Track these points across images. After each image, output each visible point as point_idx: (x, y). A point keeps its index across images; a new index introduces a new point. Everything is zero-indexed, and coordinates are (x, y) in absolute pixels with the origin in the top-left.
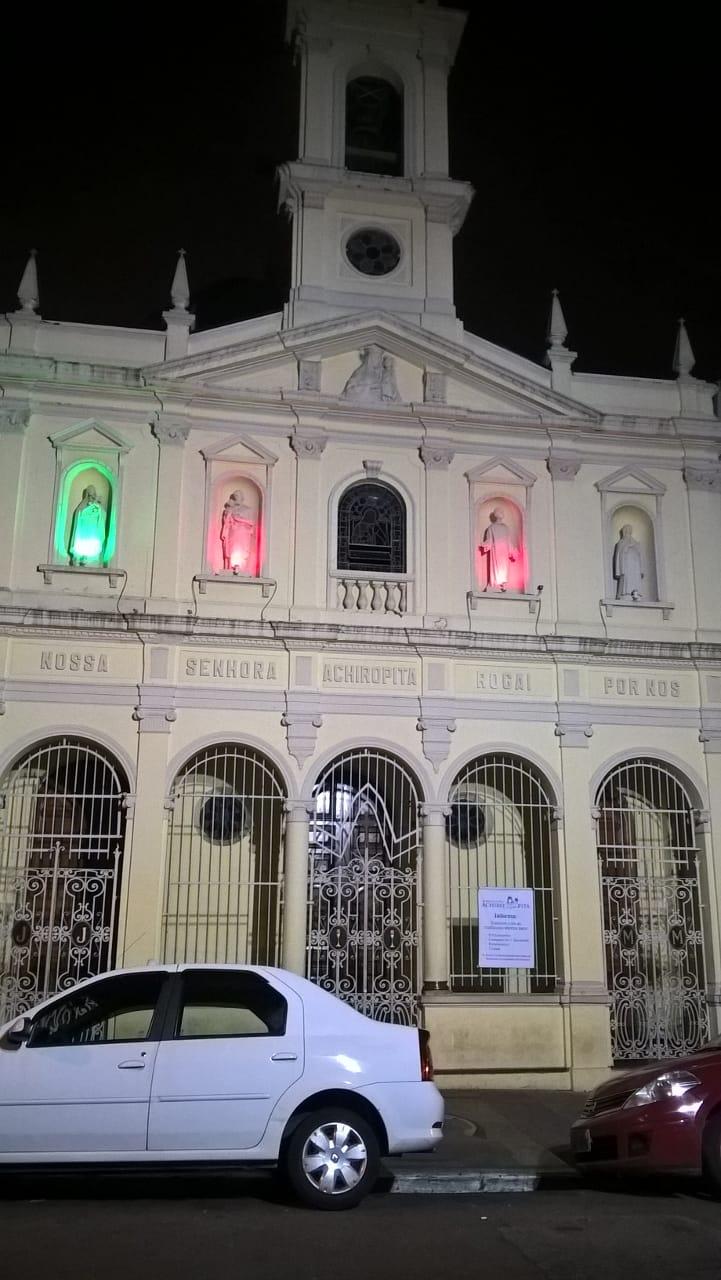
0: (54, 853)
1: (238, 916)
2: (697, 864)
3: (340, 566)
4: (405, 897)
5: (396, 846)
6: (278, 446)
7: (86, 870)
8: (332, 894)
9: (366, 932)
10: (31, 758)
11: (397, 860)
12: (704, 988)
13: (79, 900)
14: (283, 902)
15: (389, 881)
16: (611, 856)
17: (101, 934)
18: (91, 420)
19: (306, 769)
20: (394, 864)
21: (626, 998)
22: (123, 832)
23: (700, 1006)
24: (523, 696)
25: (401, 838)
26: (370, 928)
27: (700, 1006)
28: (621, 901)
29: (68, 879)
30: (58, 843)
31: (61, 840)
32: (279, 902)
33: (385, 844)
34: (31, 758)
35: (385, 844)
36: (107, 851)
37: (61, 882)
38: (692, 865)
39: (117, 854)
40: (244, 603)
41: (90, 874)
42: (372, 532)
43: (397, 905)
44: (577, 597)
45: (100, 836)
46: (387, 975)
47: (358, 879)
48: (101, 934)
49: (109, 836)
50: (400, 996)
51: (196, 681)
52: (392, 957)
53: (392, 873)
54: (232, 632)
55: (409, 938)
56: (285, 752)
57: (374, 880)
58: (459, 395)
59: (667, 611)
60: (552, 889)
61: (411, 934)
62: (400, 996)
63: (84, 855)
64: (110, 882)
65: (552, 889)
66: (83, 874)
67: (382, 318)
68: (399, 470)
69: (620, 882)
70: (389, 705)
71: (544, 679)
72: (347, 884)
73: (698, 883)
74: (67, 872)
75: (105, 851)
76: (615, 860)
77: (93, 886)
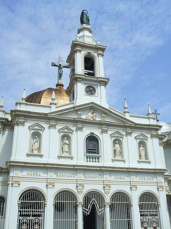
0: (30, 214)
2: (158, 213)
5: (100, 211)
6: (149, 136)
13: (36, 224)
16: (23, 212)
18: (65, 125)
19: (108, 196)
22: (44, 209)
25: (101, 210)
26: (151, 227)
28: (144, 221)
30: (31, 212)
31: (31, 211)
32: (18, 223)
37: (32, 220)
38: (157, 213)
39: (43, 214)
43: (26, 224)
45: (39, 210)
49: (30, 210)
64: (42, 220)
68: (97, 132)
69: (144, 218)
70: (41, 180)
72: (26, 219)
74: (151, 217)
76: (35, 213)
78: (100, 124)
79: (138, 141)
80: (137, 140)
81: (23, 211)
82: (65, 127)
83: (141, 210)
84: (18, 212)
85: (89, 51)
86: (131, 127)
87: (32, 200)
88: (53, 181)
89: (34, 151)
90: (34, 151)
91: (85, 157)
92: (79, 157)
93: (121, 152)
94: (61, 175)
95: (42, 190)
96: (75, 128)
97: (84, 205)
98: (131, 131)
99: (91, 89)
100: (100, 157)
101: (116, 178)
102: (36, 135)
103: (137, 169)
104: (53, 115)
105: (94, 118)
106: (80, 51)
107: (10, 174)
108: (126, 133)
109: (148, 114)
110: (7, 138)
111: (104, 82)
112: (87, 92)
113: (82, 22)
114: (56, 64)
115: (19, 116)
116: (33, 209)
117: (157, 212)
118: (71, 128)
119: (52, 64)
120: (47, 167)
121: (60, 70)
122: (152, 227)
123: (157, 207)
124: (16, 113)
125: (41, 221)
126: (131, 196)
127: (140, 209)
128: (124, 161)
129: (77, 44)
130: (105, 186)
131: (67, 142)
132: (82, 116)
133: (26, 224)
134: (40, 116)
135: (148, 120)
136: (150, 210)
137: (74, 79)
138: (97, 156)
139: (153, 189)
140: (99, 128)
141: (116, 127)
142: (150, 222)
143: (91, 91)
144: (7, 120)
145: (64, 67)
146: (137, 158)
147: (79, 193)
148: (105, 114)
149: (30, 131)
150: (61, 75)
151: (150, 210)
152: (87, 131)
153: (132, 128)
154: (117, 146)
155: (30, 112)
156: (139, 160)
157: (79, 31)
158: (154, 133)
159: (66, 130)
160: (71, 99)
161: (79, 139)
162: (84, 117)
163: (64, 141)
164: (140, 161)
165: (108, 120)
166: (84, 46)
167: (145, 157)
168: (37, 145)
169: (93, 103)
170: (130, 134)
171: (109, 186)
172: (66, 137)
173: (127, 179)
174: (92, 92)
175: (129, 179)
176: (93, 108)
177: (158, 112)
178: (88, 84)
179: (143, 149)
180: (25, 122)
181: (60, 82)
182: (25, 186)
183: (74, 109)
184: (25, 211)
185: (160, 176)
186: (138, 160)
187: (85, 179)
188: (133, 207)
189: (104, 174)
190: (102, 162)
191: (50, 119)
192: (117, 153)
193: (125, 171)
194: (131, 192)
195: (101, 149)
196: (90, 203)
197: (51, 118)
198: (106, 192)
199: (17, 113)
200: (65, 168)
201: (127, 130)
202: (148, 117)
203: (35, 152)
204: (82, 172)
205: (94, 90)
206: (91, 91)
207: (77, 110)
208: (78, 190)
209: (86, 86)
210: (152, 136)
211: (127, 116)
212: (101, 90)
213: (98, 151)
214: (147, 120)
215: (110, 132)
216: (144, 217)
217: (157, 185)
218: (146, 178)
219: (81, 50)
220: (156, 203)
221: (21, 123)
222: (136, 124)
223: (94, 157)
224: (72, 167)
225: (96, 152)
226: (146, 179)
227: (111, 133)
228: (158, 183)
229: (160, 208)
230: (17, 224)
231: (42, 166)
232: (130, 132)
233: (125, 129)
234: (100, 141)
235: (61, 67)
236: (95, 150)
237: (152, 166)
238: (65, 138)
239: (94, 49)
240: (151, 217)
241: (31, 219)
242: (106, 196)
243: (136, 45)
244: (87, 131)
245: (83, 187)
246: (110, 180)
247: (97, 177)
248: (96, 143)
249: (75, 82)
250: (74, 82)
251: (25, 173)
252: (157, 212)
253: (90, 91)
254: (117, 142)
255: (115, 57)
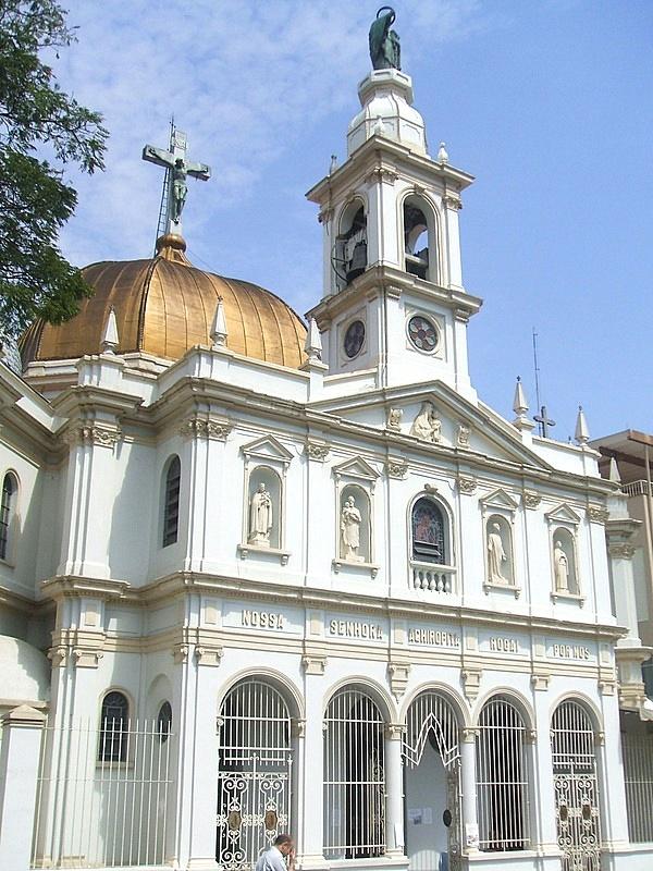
2: (595, 764)
19: (401, 703)
68: (444, 488)
72: (240, 779)
78: (453, 461)
79: (252, 465)
80: (337, 480)
82: (261, 440)
83: (225, 748)
85: (420, 185)
86: (538, 481)
87: (256, 708)
88: (323, 652)
89: (259, 537)
90: (259, 537)
91: (411, 571)
92: (393, 574)
93: (507, 563)
94: (343, 631)
95: (288, 680)
96: (301, 448)
97: (482, 735)
98: (535, 493)
99: (425, 327)
100: (453, 576)
101: (571, 654)
102: (265, 480)
103: (554, 622)
104: (321, 412)
105: (436, 433)
106: (393, 177)
107: (186, 620)
108: (306, 450)
109: (580, 439)
110: (126, 474)
111: (459, 309)
112: (413, 336)
113: (378, 57)
114: (163, 156)
115: (208, 401)
117: (287, 759)
118: (280, 441)
119: (148, 154)
120: (303, 602)
121: (177, 183)
123: (291, 734)
124: (206, 390)
126: (529, 706)
127: (222, 745)
128: (372, 572)
129: (386, 151)
130: (200, 650)
131: (355, 511)
132: (401, 426)
134: (282, 410)
135: (578, 458)
136: (261, 748)
137: (377, 283)
138: (440, 570)
139: (587, 689)
140: (450, 474)
141: (429, 460)
142: (257, 792)
143: (423, 334)
144: (138, 401)
145: (190, 172)
146: (238, 537)
147: (394, 694)
148: (467, 426)
149: (246, 462)
150: (179, 204)
151: (261, 748)
152: (412, 485)
153: (476, 468)
154: (496, 538)
155: (249, 394)
156: (245, 545)
157: (368, 92)
158: (595, 505)
159: (354, 472)
160: (334, 346)
161: (393, 500)
162: (405, 428)
163: (349, 510)
164: (250, 551)
165: (474, 447)
166: (405, 162)
167: (569, 585)
168: (263, 520)
169: (438, 384)
170: (321, 453)
171: (477, 673)
172: (354, 495)
173: (290, 627)
174: (427, 338)
175: (300, 628)
176: (433, 399)
177: (549, 416)
178: (421, 309)
179: (564, 555)
180: (232, 427)
181: (176, 232)
182: (237, 663)
183: (384, 397)
185: (606, 650)
186: (242, 547)
187: (411, 648)
188: (536, 745)
189: (308, 617)
190: (456, 593)
191: (307, 425)
192: (501, 564)
193: (377, 609)
194: (304, 680)
195: (454, 547)
196: (423, 726)
197: (393, 441)
198: (469, 693)
199: (208, 391)
200: (361, 607)
201: (391, 456)
202: (580, 449)
203: (263, 543)
204: (219, 601)
205: (433, 332)
206: (423, 334)
207: (386, 401)
208: (394, 684)
209: (410, 316)
210: (590, 517)
211: (527, 439)
212: (455, 336)
213: (443, 551)
214: (576, 459)
215: (333, 459)
216: (267, 774)
217: (597, 676)
218: (573, 654)
219: (394, 174)
220: (287, 722)
221: (218, 431)
222: (555, 473)
223: (440, 575)
224: (380, 607)
225: (436, 556)
226: (571, 657)
227: (246, 440)
228: (201, 633)
229: (301, 740)
231: (292, 595)
232: (322, 448)
233: (583, 498)
234: (453, 518)
235: (184, 171)
236: (436, 548)
237: (517, 607)
238: (351, 497)
239: (430, 178)
240: (577, 777)
242: (395, 702)
243: (294, 58)
244: (412, 485)
245: (218, 658)
246: (221, 629)
247: (444, 644)
248: (435, 525)
249: (378, 295)
250: (374, 293)
251: (233, 619)
252: (287, 759)
253: (422, 334)
254: (496, 525)
255: (205, 88)
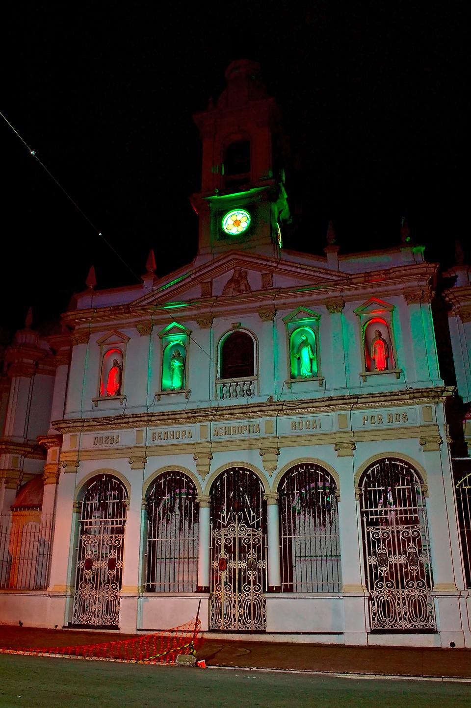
1: (32, 560)
3: (253, 375)
4: (388, 538)
5: (253, 517)
7: (410, 526)
8: (220, 542)
9: (397, 556)
10: (371, 469)
11: (253, 525)
12: (235, 592)
14: (280, 546)
15: (249, 535)
16: (372, 515)
17: (372, 560)
20: (253, 526)
21: (382, 594)
23: (233, 601)
24: (406, 424)
27: (233, 601)
28: (378, 540)
29: (243, 538)
33: (248, 516)
34: (371, 469)
35: (248, 516)
36: (370, 517)
40: (177, 404)
41: (412, 527)
42: (238, 359)
44: (345, 372)
46: (249, 584)
47: (233, 535)
48: (372, 560)
50: (256, 594)
51: (157, 443)
52: (413, 569)
53: (251, 531)
54: (169, 417)
55: (423, 559)
56: (196, 473)
57: (242, 535)
58: (280, 281)
59: (399, 374)
60: (148, 540)
61: (393, 557)
62: (420, 590)
63: (411, 518)
65: (148, 540)
66: (408, 528)
67: (235, 254)
70: (176, 449)
71: (329, 420)
72: (228, 537)
73: (79, 537)
74: (371, 528)
75: (86, 527)
77: (385, 535)
81: (371, 512)
84: (362, 516)
116: (83, 519)
122: (118, 570)
123: (121, 509)
125: (261, 541)
133: (384, 541)
139: (406, 449)
142: (399, 540)
182: (90, 468)
184: (376, 514)
230: (281, 548)
241: (395, 529)
